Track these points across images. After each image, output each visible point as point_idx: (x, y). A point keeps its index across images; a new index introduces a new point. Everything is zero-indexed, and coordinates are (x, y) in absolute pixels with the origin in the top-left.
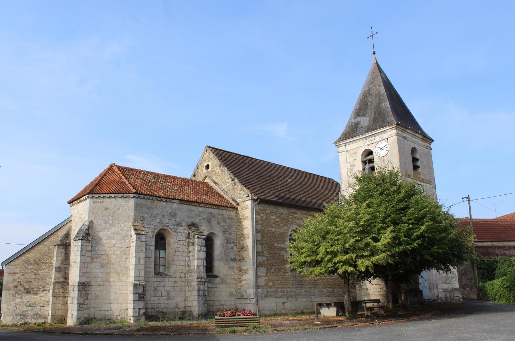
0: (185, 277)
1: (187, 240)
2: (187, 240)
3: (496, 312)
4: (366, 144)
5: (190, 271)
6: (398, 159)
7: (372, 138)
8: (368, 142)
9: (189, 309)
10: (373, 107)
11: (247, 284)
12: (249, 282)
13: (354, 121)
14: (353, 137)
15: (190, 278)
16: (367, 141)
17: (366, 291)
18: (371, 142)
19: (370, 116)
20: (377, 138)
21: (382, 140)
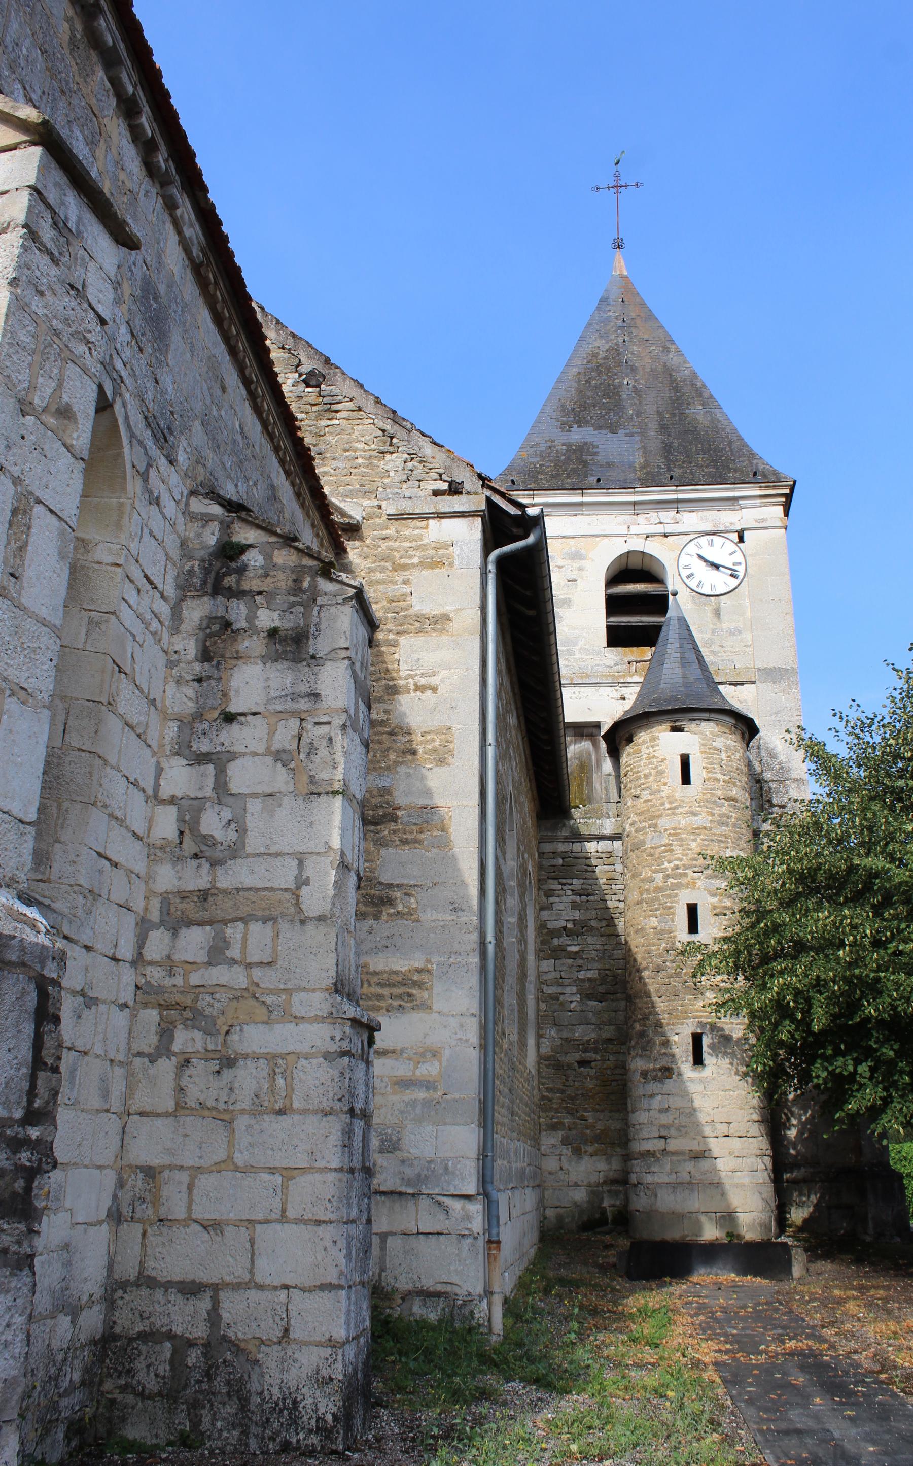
0: (138, 961)
1: (196, 611)
2: (196, 611)
3: (859, 1261)
4: (634, 529)
5: (222, 908)
6: (790, 619)
7: (667, 515)
8: (646, 523)
9: (185, 1318)
10: (650, 409)
11: (405, 1084)
12: (429, 1069)
13: (561, 439)
14: (581, 489)
15: (219, 975)
16: (641, 519)
17: (689, 1166)
18: (660, 529)
19: (643, 434)
20: (691, 520)
21: (714, 533)
